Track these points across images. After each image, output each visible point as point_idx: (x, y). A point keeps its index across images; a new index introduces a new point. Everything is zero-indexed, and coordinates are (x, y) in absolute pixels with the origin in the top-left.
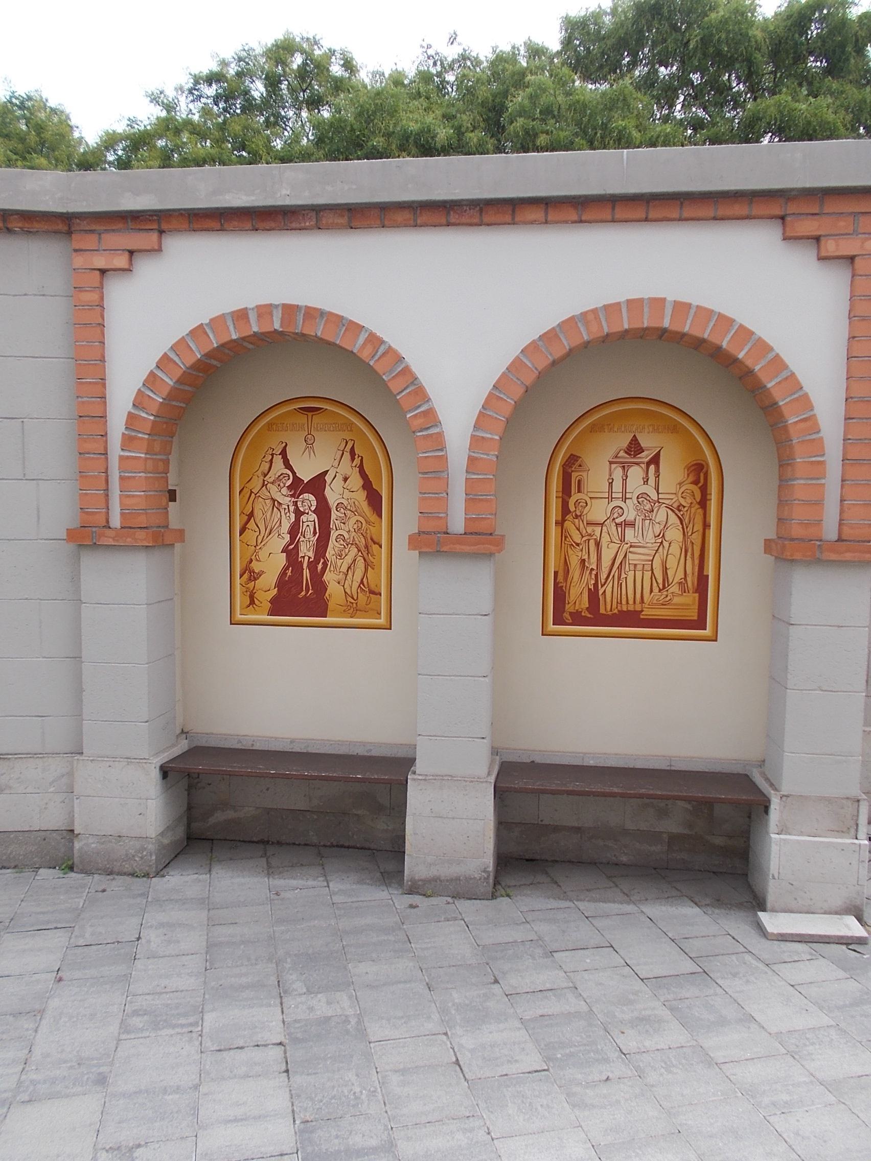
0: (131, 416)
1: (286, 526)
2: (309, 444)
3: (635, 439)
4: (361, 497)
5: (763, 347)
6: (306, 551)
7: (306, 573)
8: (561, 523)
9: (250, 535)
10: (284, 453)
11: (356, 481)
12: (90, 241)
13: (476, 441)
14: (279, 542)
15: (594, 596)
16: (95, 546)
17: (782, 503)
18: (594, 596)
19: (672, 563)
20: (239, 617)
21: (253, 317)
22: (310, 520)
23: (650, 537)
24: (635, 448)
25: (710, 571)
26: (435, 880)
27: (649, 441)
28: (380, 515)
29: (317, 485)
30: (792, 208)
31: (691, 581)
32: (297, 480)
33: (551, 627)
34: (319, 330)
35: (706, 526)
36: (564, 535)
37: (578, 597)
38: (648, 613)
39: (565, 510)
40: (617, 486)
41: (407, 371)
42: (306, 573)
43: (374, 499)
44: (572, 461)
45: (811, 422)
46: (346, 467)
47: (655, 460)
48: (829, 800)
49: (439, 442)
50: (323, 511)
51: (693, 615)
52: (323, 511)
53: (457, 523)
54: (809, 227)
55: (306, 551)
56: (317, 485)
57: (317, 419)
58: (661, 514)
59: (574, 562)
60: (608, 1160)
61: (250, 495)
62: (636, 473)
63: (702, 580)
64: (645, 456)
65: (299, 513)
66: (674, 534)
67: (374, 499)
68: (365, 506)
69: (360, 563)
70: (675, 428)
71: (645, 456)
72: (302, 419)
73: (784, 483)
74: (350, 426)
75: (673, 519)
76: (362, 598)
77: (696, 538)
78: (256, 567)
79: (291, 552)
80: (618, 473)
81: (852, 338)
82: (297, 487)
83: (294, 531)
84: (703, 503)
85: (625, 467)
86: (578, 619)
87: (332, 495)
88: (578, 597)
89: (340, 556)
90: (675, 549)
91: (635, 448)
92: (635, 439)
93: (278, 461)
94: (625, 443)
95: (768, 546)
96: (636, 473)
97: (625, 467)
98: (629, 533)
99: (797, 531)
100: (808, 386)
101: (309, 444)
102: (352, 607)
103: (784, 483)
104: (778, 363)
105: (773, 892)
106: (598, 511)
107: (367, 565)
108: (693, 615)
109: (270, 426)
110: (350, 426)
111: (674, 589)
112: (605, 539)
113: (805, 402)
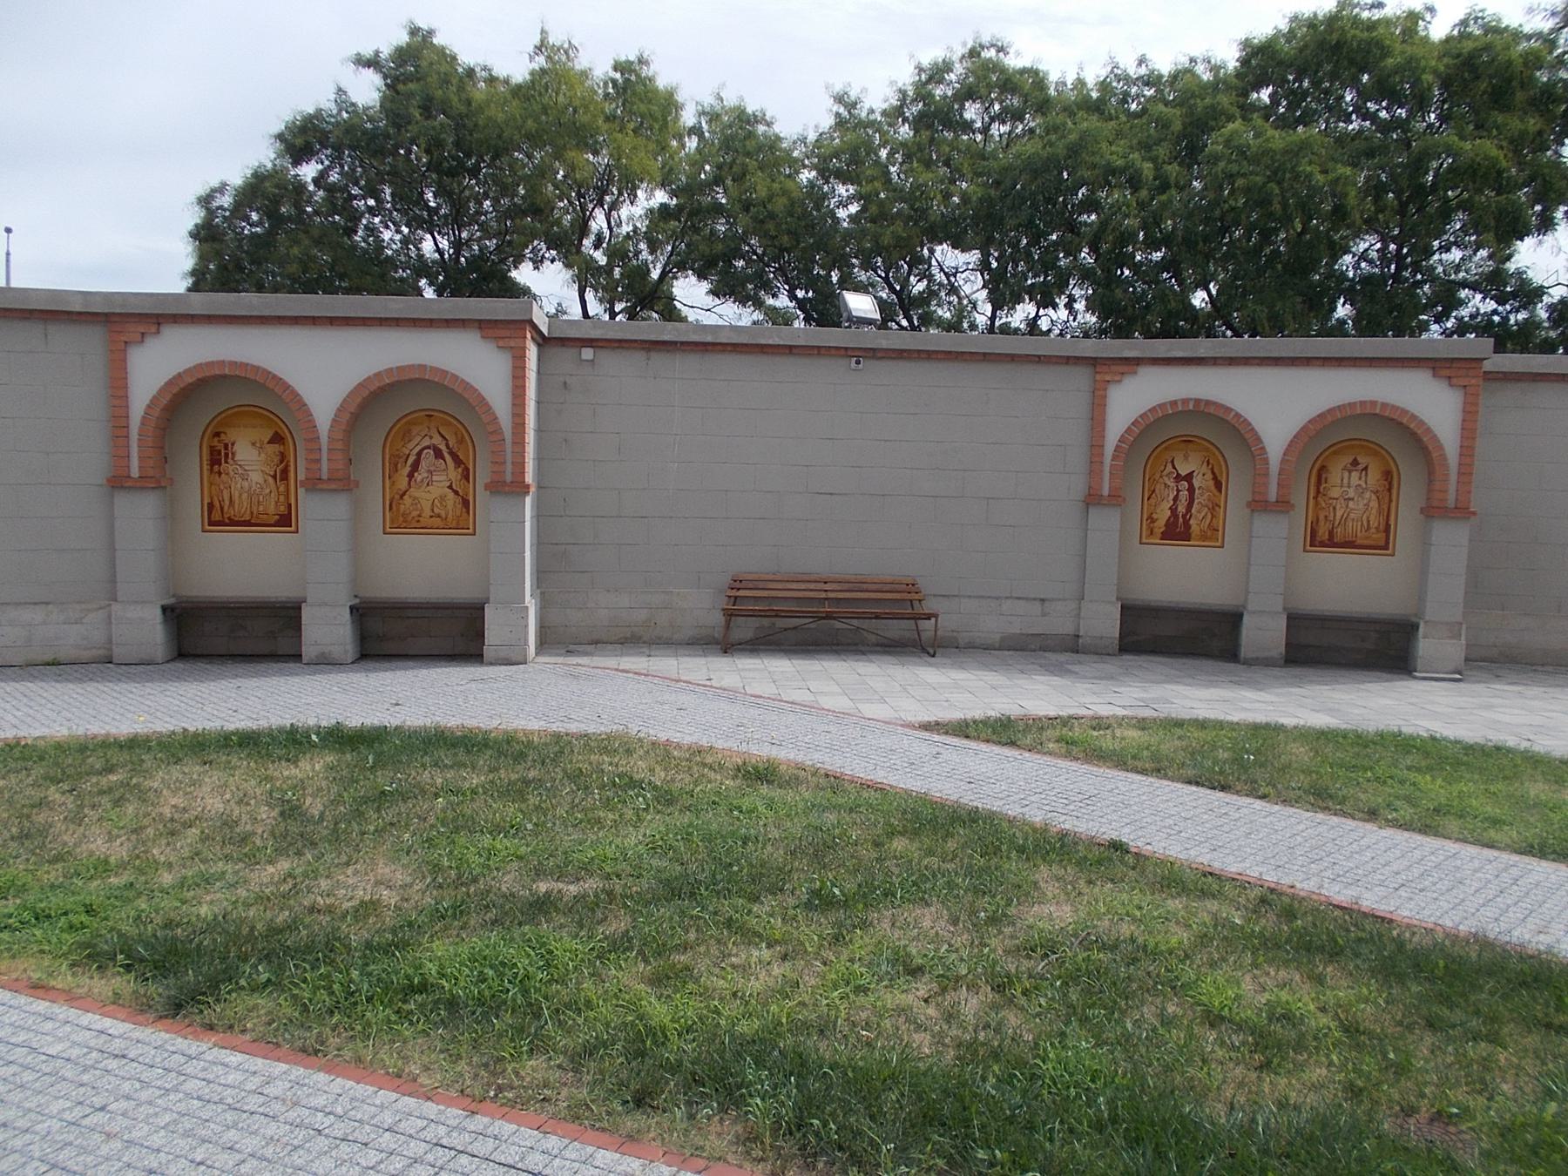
0: (1117, 446)
1: (1171, 497)
2: (1186, 457)
3: (1355, 459)
4: (1211, 483)
5: (1422, 423)
6: (1181, 509)
7: (1181, 520)
8: (1315, 498)
9: (1152, 501)
10: (1172, 462)
11: (1209, 476)
12: (1105, 368)
13: (1283, 461)
14: (1169, 503)
15: (1331, 533)
16: (122, 487)
17: (1429, 491)
18: (1331, 533)
19: (1372, 518)
20: (1144, 540)
21: (1179, 403)
22: (1184, 494)
23: (1361, 506)
24: (1355, 463)
25: (1392, 522)
26: (1257, 659)
27: (1363, 460)
28: (1220, 491)
29: (1189, 477)
30: (1438, 364)
31: (1382, 527)
32: (1178, 475)
33: (1308, 548)
34: (1212, 410)
35: (1390, 501)
36: (1317, 504)
37: (1323, 533)
38: (1359, 542)
39: (1318, 492)
40: (1345, 481)
41: (1253, 429)
42: (1181, 520)
43: (1218, 485)
44: (1323, 469)
45: (1443, 457)
46: (1204, 469)
47: (1366, 469)
48: (1447, 623)
49: (1266, 461)
50: (1191, 490)
51: (1382, 543)
52: (1191, 490)
53: (1273, 495)
54: (1446, 372)
55: (1181, 509)
56: (1189, 477)
57: (1191, 445)
58: (1367, 495)
59: (1322, 517)
60: (1567, 315)
61: (1153, 480)
62: (1355, 475)
63: (1388, 526)
64: (1360, 467)
65: (1178, 491)
66: (1374, 504)
67: (1218, 485)
68: (1213, 488)
69: (1209, 516)
70: (1376, 454)
71: (1360, 467)
72: (1183, 445)
73: (1430, 482)
74: (1207, 450)
75: (1374, 497)
76: (1209, 533)
77: (1386, 507)
78: (1155, 516)
79: (1173, 510)
80: (1346, 474)
81: (1464, 420)
82: (1178, 478)
83: (1176, 499)
84: (1390, 490)
85: (1350, 472)
86: (1322, 544)
87: (1196, 483)
88: (1323, 533)
89: (1199, 512)
90: (1374, 511)
91: (1355, 463)
92: (1355, 459)
93: (1169, 466)
94: (1351, 460)
95: (1422, 511)
96: (1355, 475)
97: (1350, 472)
98: (1351, 504)
99: (1435, 504)
100: (1449, 456)
101: (1186, 457)
102: (1204, 537)
103: (1430, 482)
104: (1429, 430)
105: (1419, 664)
106: (1335, 493)
107: (1213, 516)
108: (1382, 543)
109: (1166, 448)
110: (1207, 450)
111: (1373, 530)
112: (1338, 507)
113: (1441, 448)
